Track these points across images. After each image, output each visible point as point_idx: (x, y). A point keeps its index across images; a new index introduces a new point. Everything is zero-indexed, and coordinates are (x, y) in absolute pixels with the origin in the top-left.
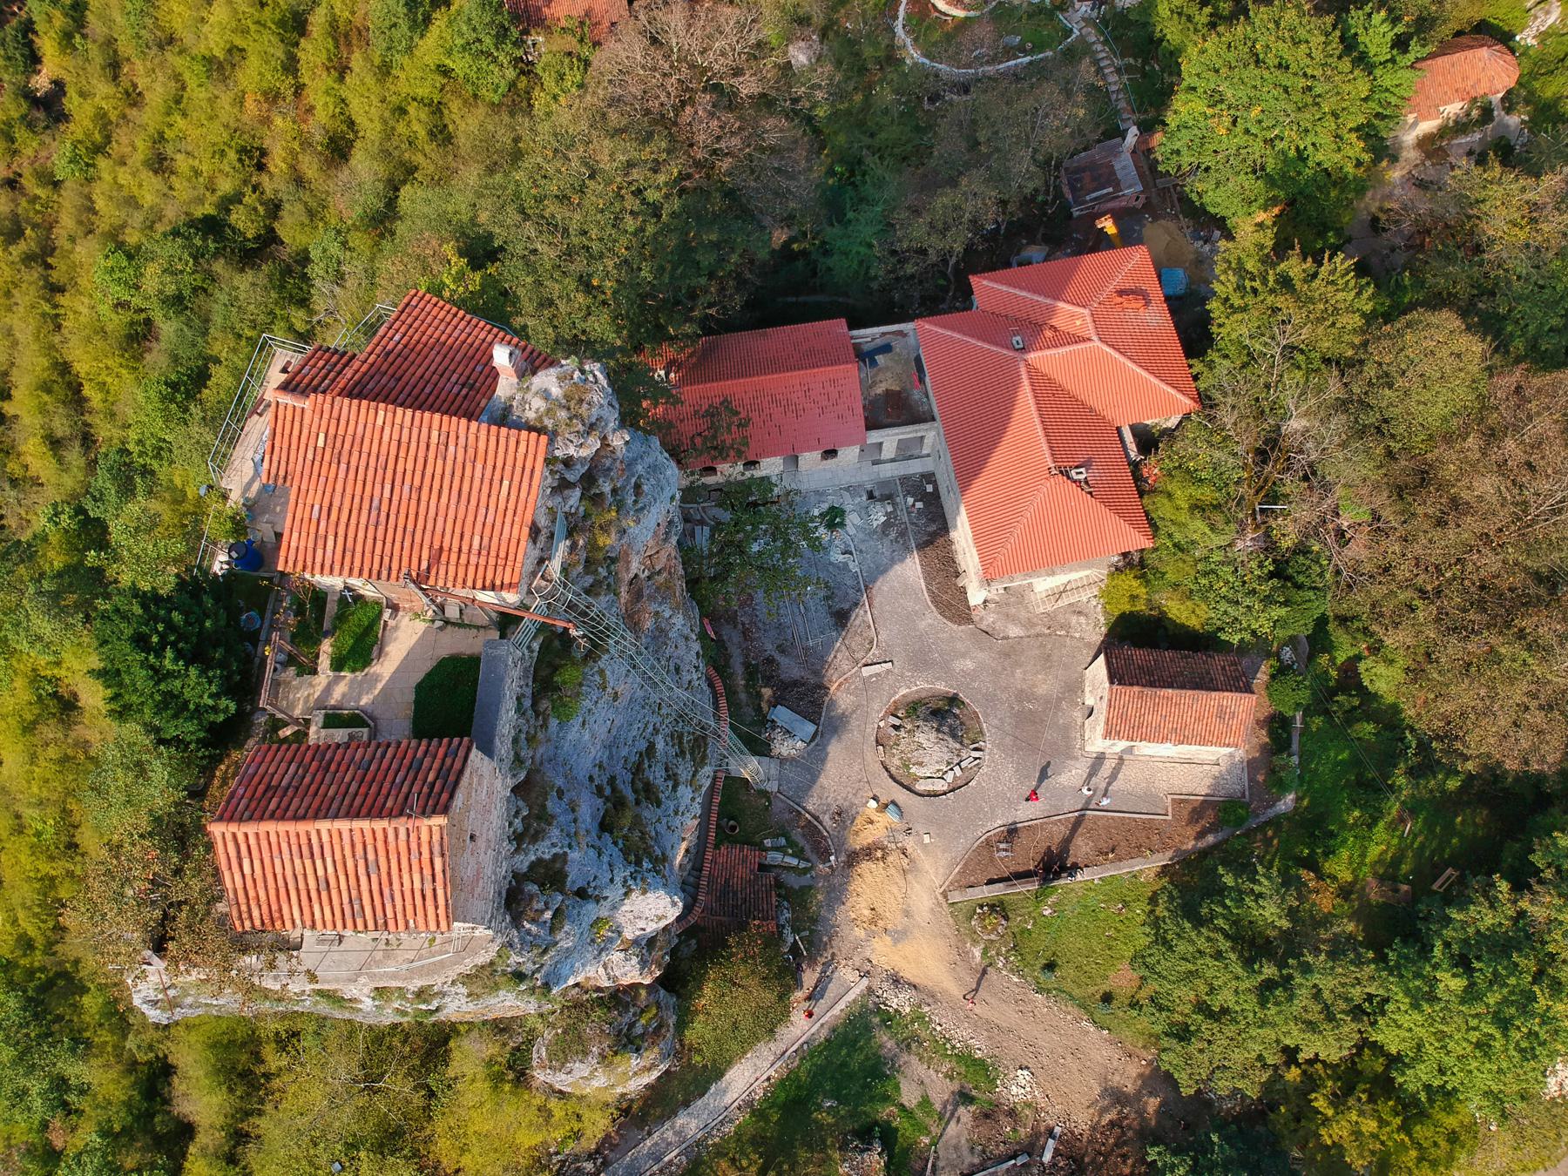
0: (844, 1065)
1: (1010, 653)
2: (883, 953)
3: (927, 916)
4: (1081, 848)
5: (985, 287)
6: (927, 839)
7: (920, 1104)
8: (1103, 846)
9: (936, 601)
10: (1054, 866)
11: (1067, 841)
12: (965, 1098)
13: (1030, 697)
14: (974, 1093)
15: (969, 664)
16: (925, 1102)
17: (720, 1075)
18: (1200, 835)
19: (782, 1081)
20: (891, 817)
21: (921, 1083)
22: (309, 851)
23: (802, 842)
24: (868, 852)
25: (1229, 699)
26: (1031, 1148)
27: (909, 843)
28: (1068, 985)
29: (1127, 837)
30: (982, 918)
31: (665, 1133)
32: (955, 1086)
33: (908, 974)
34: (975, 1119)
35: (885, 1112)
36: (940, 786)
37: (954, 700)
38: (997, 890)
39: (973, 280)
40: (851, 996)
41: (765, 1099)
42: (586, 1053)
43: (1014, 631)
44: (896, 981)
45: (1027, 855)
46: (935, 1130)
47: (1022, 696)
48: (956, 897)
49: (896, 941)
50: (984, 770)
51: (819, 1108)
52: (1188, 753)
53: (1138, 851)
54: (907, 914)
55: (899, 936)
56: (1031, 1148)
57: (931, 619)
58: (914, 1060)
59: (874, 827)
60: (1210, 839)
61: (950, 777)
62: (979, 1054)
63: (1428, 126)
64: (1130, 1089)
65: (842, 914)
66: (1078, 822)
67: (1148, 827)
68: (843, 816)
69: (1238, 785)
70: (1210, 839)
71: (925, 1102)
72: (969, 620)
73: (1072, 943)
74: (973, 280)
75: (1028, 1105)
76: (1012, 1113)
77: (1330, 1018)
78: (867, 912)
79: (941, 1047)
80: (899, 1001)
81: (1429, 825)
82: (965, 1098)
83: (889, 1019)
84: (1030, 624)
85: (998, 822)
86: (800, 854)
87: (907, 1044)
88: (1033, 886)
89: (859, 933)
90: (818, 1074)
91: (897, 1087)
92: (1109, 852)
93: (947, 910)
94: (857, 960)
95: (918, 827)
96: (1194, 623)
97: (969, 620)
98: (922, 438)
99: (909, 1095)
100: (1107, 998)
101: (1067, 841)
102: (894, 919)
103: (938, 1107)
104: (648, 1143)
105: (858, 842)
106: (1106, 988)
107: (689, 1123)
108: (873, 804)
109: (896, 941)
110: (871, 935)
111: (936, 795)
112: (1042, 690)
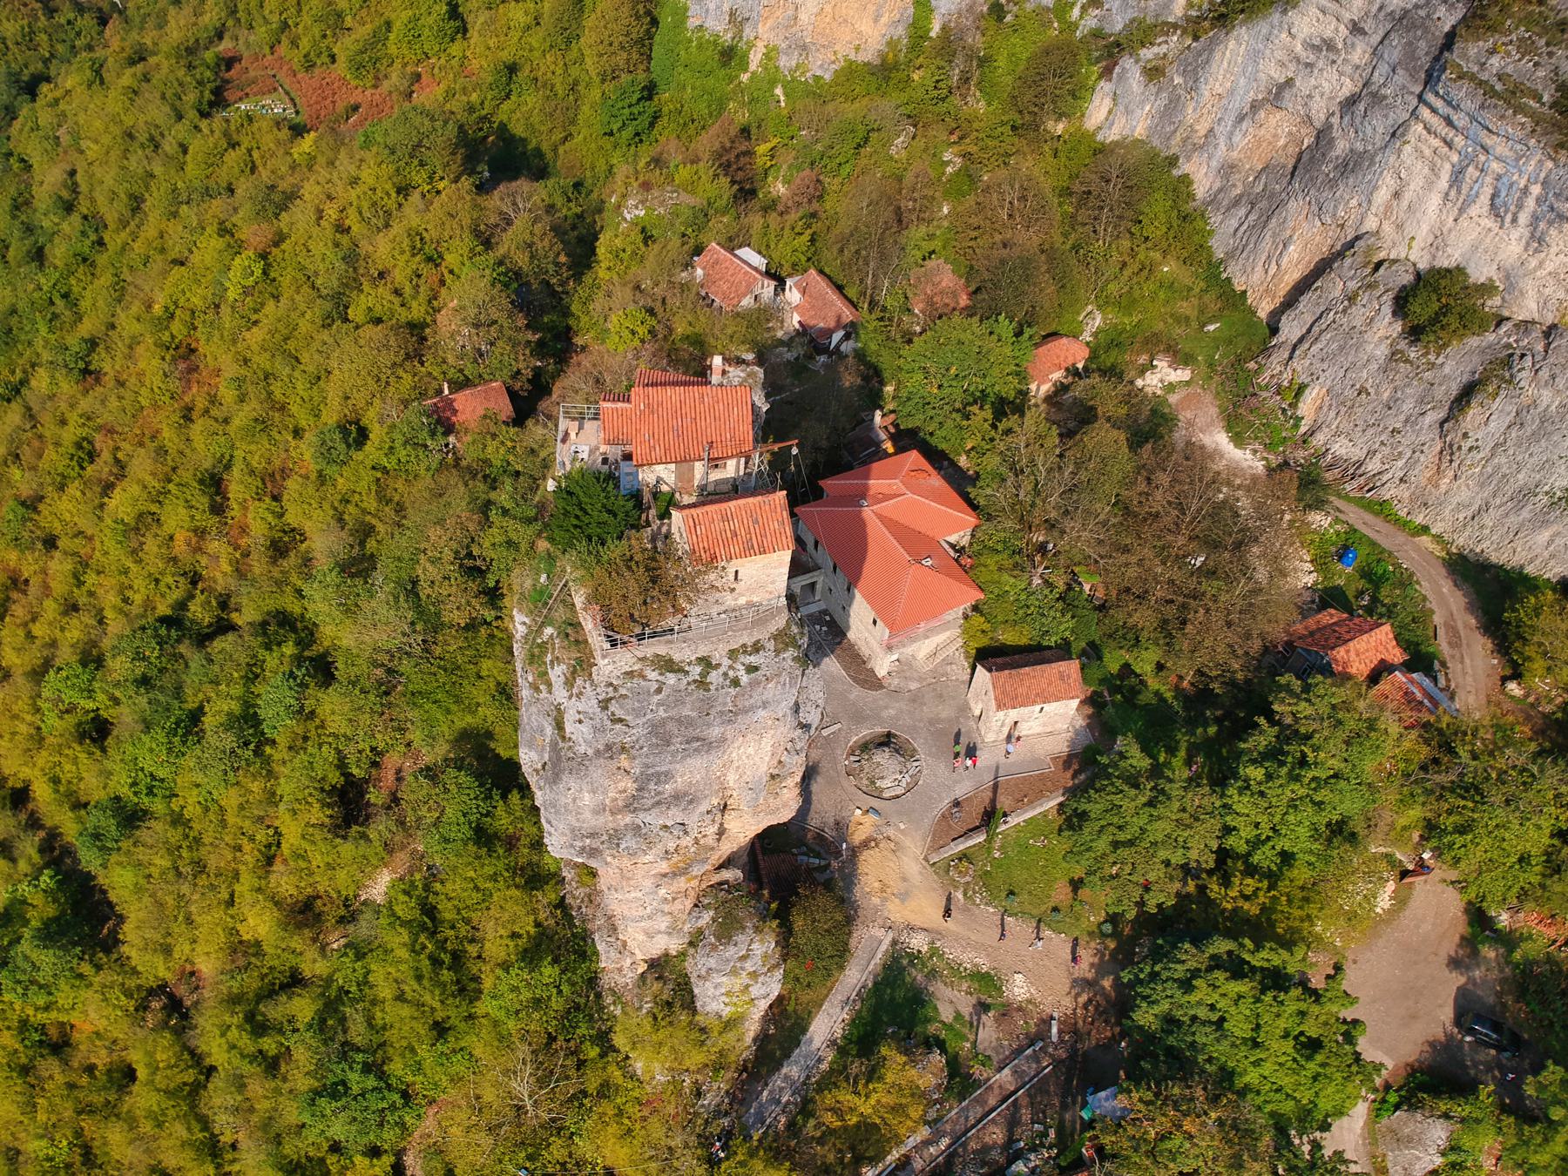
0: (892, 999)
1: (916, 698)
2: (897, 912)
3: (919, 878)
4: (1004, 802)
5: (829, 484)
6: (902, 826)
7: (955, 1018)
8: (1017, 796)
9: (855, 680)
10: (990, 816)
11: (993, 801)
12: (983, 1007)
13: (939, 721)
14: (989, 1000)
15: (892, 712)
16: (958, 1016)
17: (804, 1030)
18: (1074, 777)
19: (853, 1021)
20: (872, 817)
21: (950, 1003)
22: (725, 518)
23: (817, 848)
24: (865, 844)
25: (1062, 666)
26: (1041, 1035)
27: (891, 832)
28: (1027, 907)
29: (1031, 789)
30: (956, 867)
31: (777, 1081)
32: (973, 1000)
33: (917, 921)
34: (996, 1020)
35: (932, 1029)
36: (899, 791)
37: (889, 735)
38: (962, 846)
39: (821, 483)
40: (884, 947)
41: (844, 1037)
42: (744, 928)
43: (913, 686)
44: (912, 928)
45: (974, 815)
46: (972, 1037)
47: (932, 722)
48: (934, 858)
49: (903, 901)
50: (925, 772)
51: (892, 999)
52: (1050, 719)
53: (1040, 795)
54: (904, 879)
55: (904, 896)
56: (1041, 1035)
57: (856, 692)
58: (940, 985)
59: (862, 825)
60: (1082, 777)
61: (904, 784)
62: (985, 969)
63: (1046, 388)
64: (1090, 975)
65: (858, 892)
66: (995, 787)
67: (1042, 778)
68: (840, 826)
69: (1086, 739)
70: (1082, 777)
71: (958, 1016)
72: (881, 687)
73: (1019, 875)
74: (821, 483)
75: (1029, 1001)
76: (1020, 1009)
77: (1196, 819)
78: (877, 884)
79: (955, 969)
80: (918, 942)
81: (1208, 756)
82: (983, 1007)
83: (915, 957)
84: (920, 679)
85: (946, 802)
86: (818, 856)
87: (933, 974)
88: (980, 838)
89: (876, 900)
90: (875, 1011)
91: (936, 1008)
92: (1020, 802)
93: (931, 870)
94: (880, 921)
95: (893, 820)
96: (1024, 641)
97: (881, 687)
98: (813, 585)
99: (946, 1014)
100: (1055, 909)
101: (993, 801)
102: (896, 885)
103: (967, 1018)
104: (765, 1093)
105: (858, 837)
106: (1052, 904)
107: (792, 1070)
108: (858, 812)
109: (903, 901)
110: (885, 900)
111: (898, 797)
112: (944, 715)
